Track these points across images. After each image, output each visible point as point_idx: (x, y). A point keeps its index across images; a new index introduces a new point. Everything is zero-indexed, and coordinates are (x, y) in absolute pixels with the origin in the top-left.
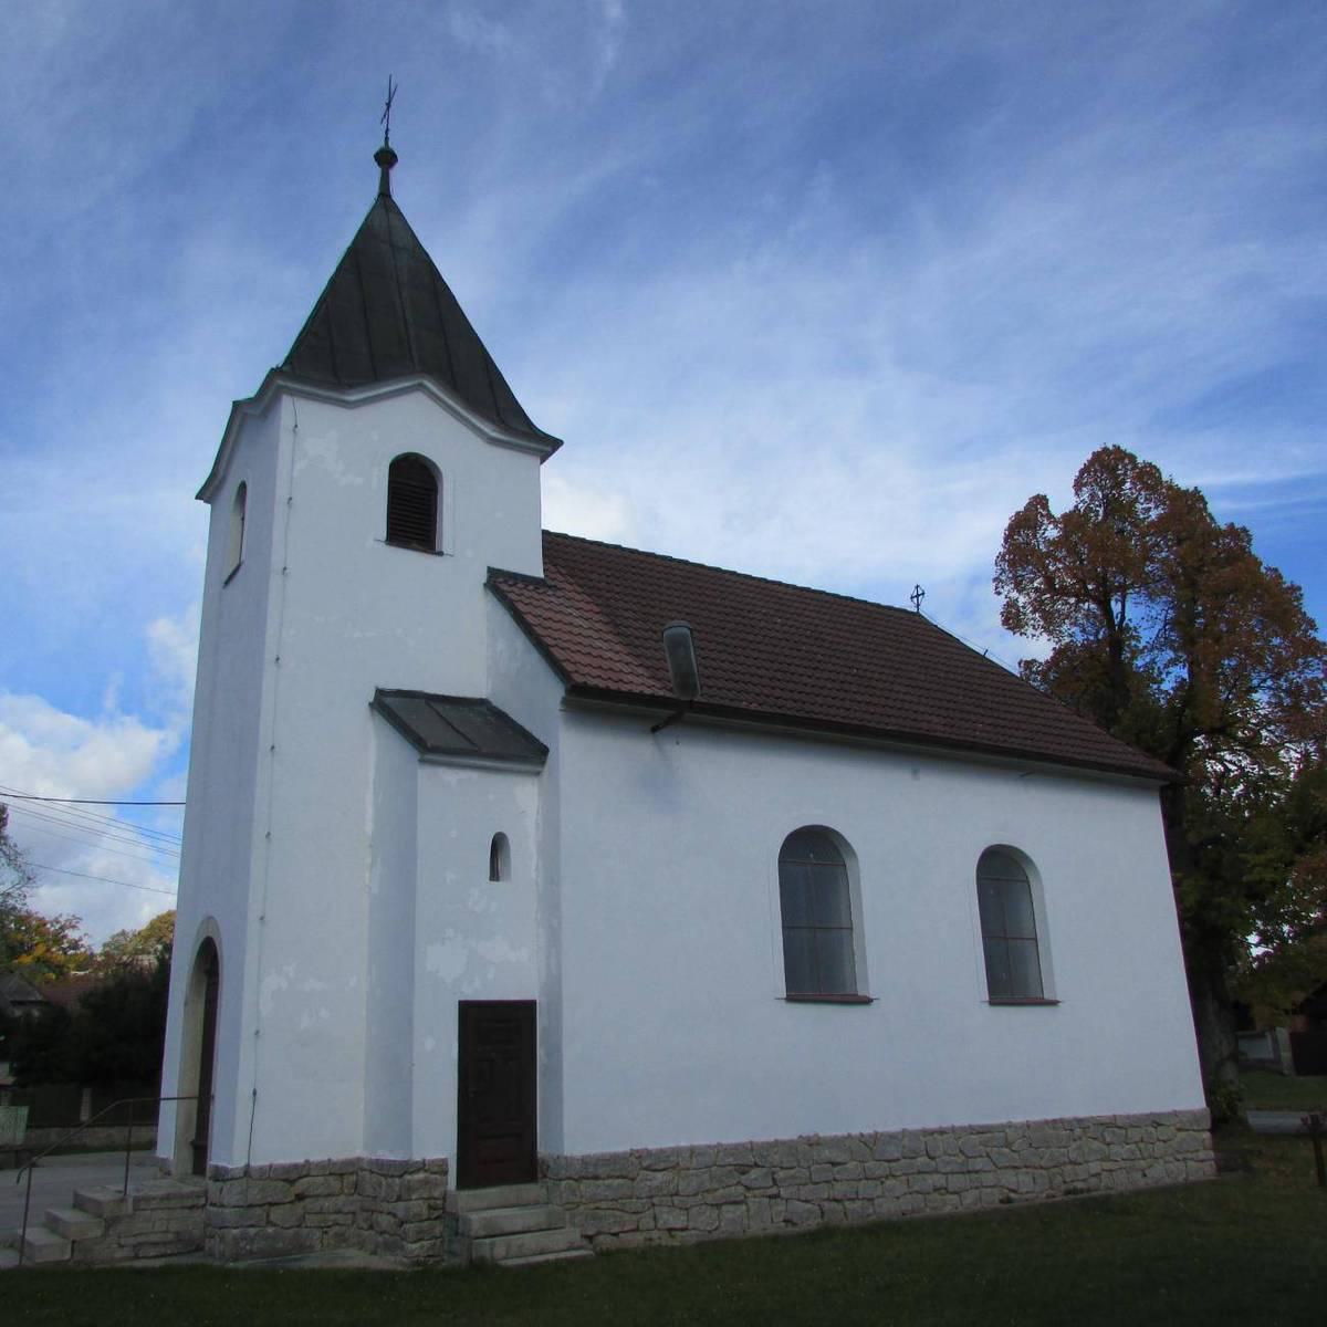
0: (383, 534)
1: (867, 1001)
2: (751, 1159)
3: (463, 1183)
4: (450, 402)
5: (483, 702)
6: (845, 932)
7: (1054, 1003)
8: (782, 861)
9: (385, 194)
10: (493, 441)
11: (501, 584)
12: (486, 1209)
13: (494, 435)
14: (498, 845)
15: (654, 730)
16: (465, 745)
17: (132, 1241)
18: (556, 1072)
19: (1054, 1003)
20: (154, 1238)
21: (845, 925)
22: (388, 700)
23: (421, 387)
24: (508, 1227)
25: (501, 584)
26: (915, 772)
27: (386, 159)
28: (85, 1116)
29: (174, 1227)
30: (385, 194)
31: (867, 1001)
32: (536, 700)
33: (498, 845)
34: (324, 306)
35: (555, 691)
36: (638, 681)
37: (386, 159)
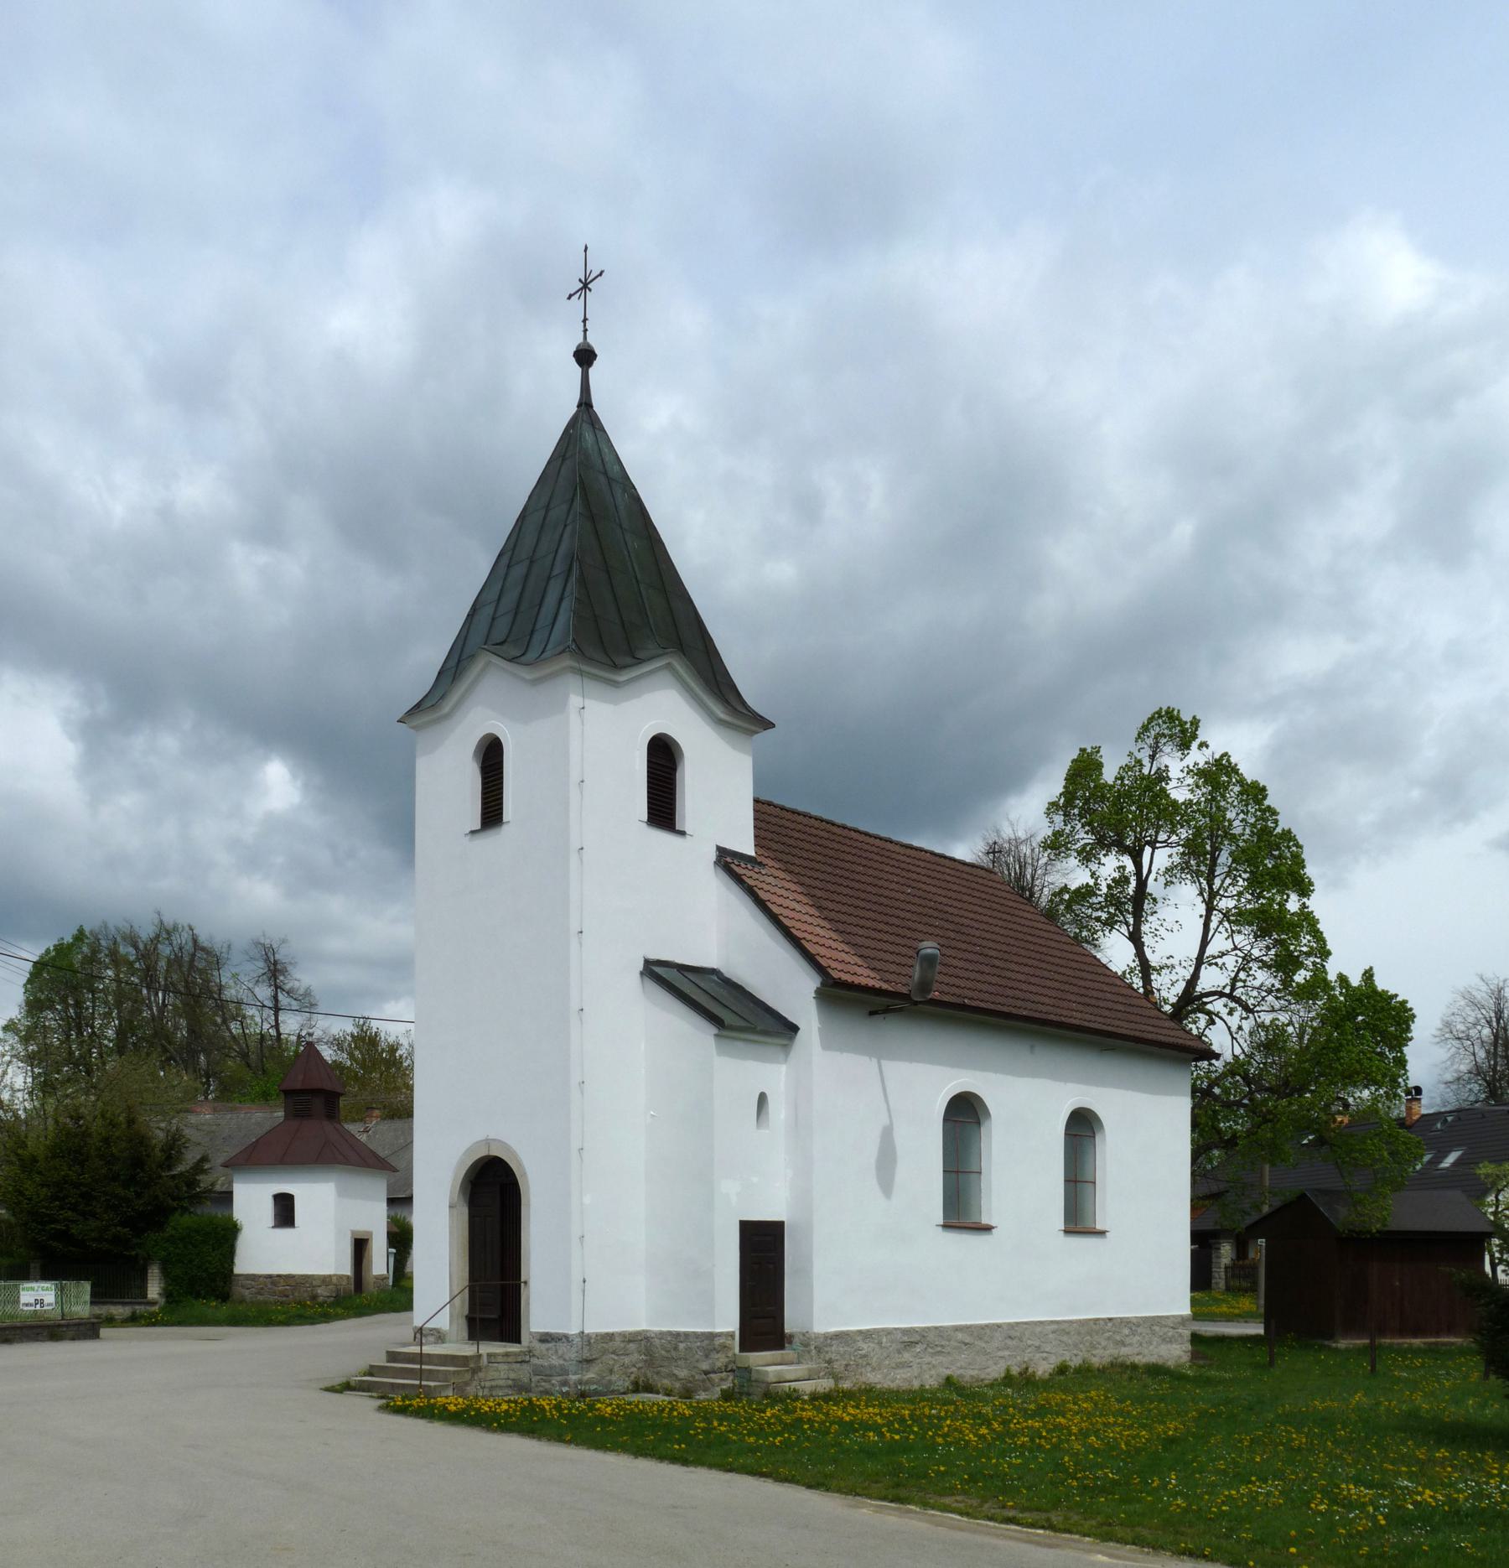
0: (645, 817)
1: (988, 1229)
2: (916, 1338)
3: (743, 1348)
4: (693, 685)
5: (714, 971)
6: (973, 1176)
7: (1102, 1233)
8: (946, 1120)
9: (585, 403)
10: (720, 722)
11: (726, 860)
12: (768, 1365)
13: (722, 716)
14: (762, 1099)
15: (872, 1013)
16: (743, 1023)
17: (488, 1384)
18: (806, 1272)
19: (1102, 1233)
20: (501, 1383)
21: (975, 1169)
22: (658, 970)
23: (669, 666)
24: (788, 1377)
25: (726, 860)
26: (1032, 1047)
27: (585, 357)
28: (154, 1290)
29: (512, 1376)
30: (585, 403)
31: (988, 1229)
32: (789, 986)
33: (762, 1099)
34: (575, 566)
35: (808, 983)
36: (866, 977)
37: (585, 357)
